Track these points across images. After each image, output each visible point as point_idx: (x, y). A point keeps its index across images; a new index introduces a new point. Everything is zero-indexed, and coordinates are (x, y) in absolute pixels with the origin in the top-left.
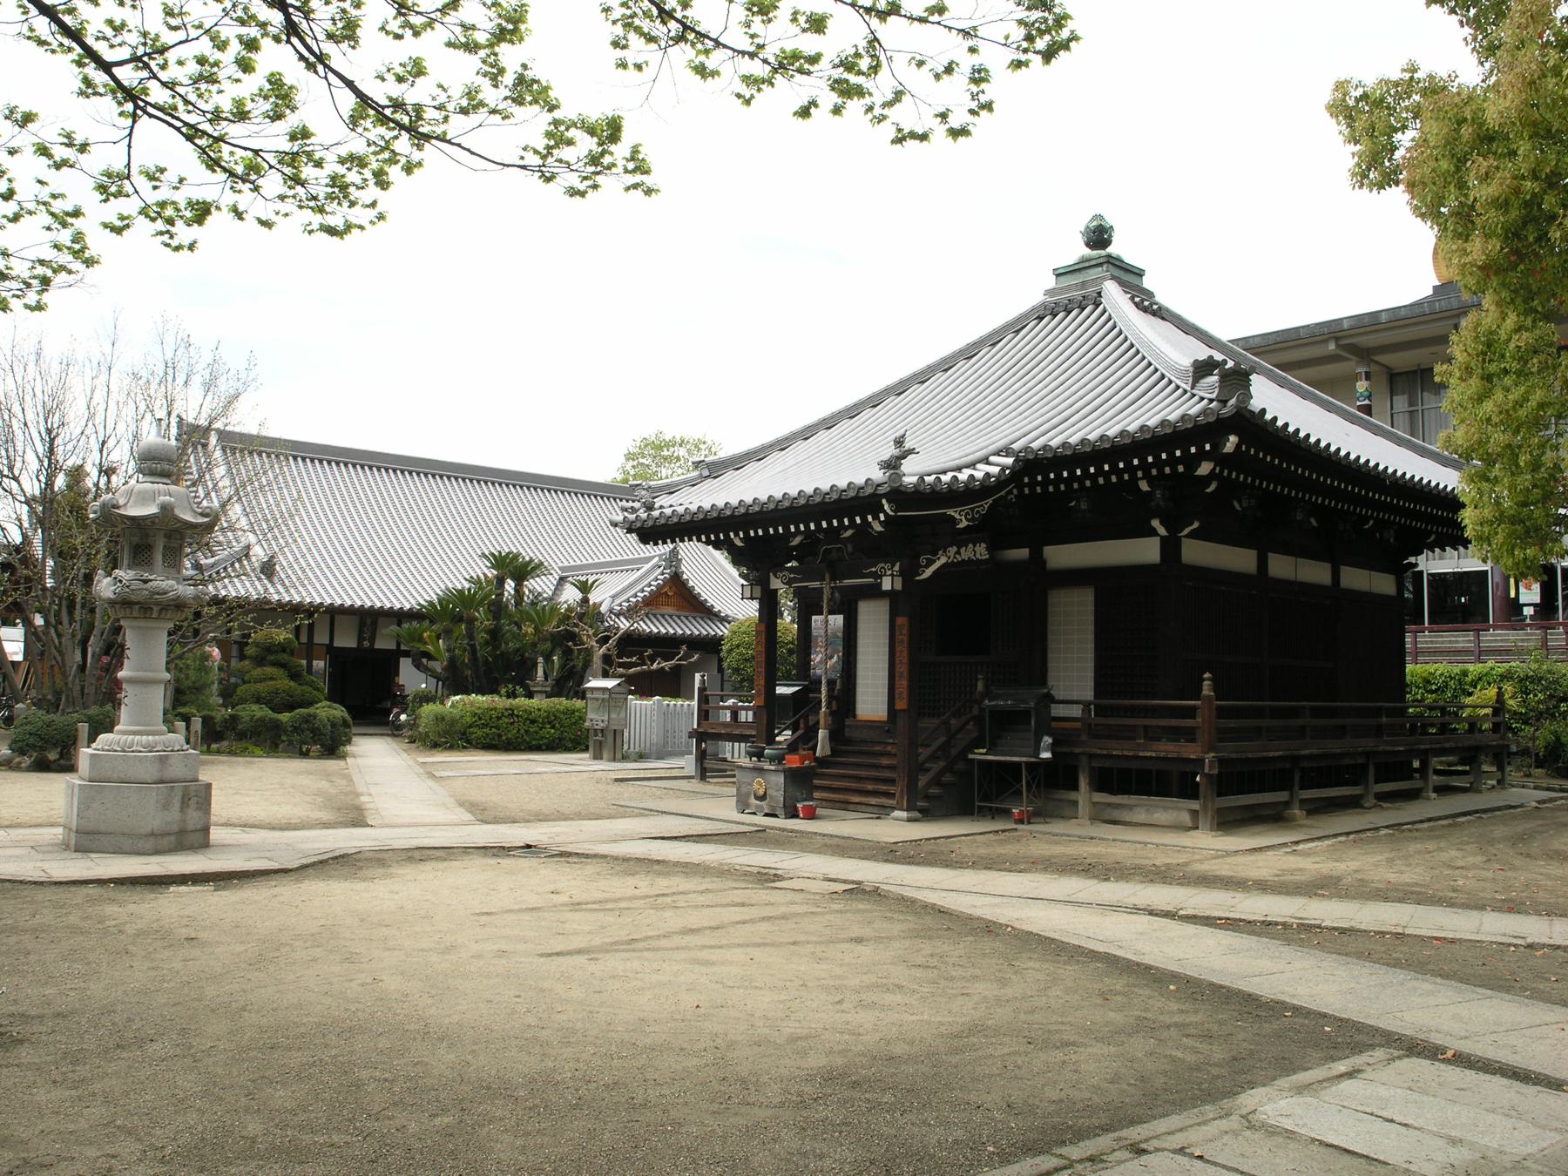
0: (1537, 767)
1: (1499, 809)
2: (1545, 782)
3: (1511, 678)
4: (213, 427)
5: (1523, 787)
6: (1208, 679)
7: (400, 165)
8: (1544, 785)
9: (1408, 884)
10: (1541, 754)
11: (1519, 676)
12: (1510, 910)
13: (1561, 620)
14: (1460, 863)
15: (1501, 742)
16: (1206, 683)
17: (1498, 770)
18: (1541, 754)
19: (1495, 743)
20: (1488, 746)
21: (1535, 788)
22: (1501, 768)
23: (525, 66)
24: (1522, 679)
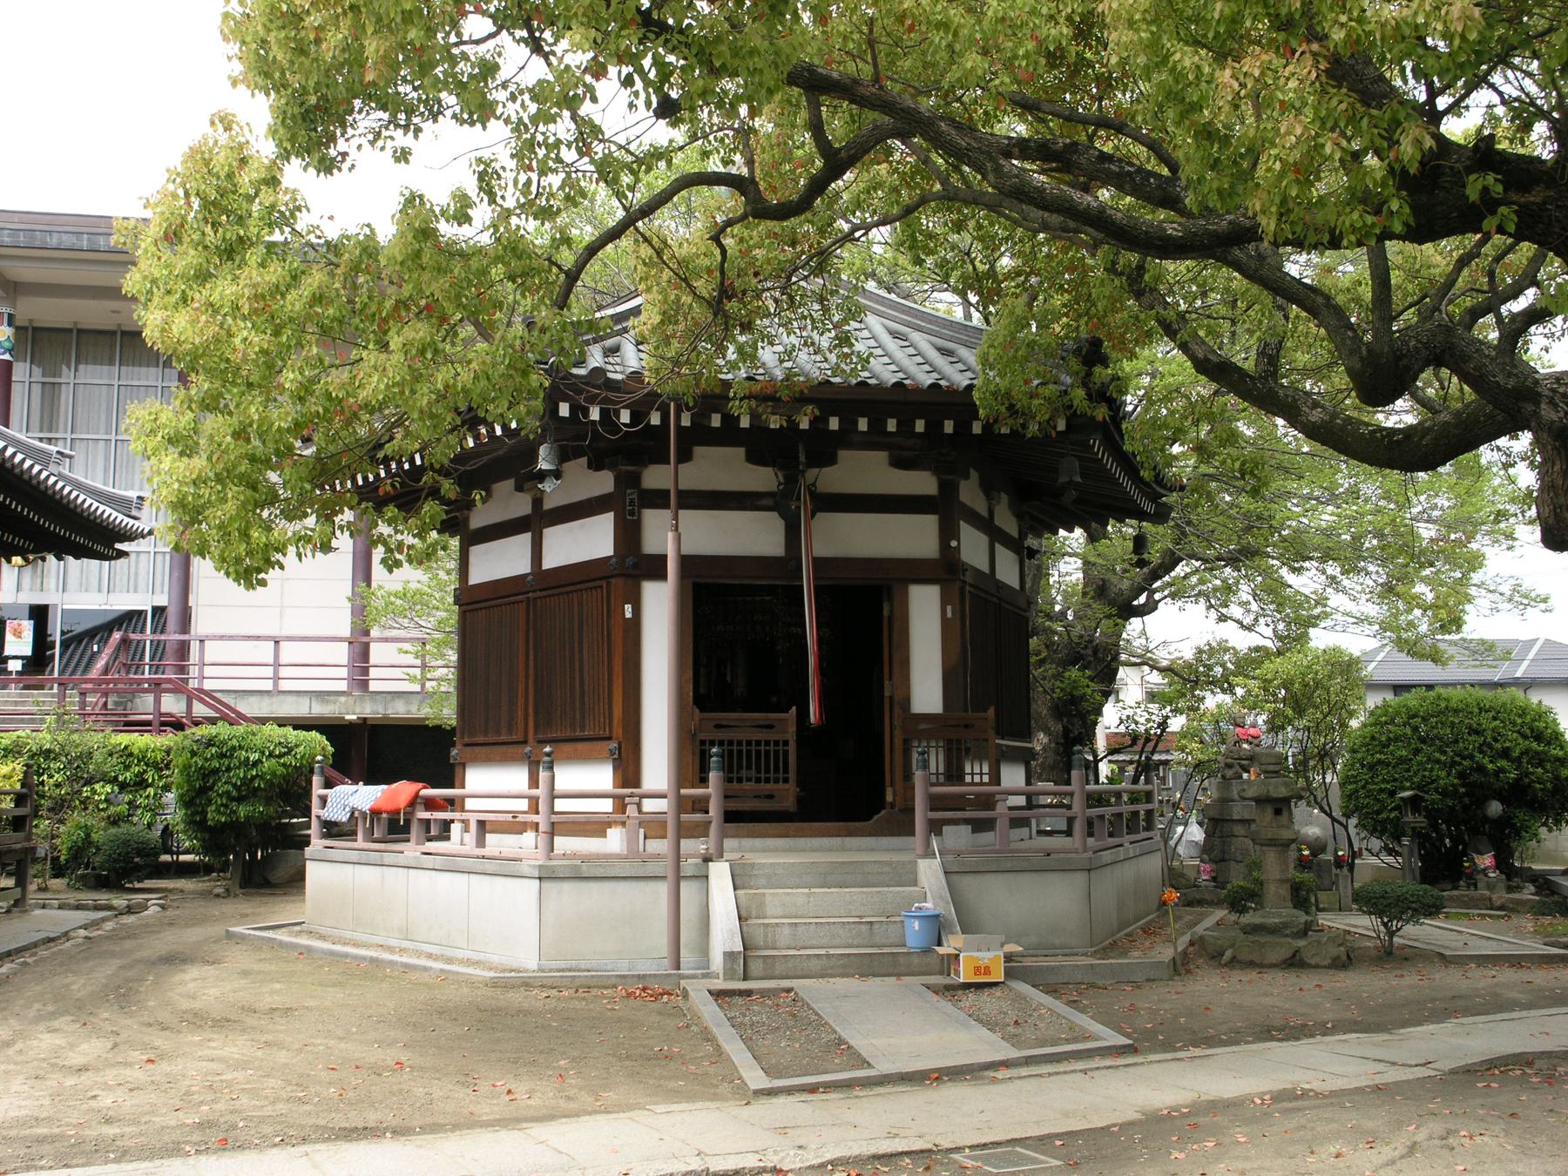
0: (56, 876)
1: (35, 945)
2: (73, 897)
3: (19, 753)
4: (1510, 241)
5: (44, 907)
6: (716, 755)
7: (594, 83)
8: (72, 901)
9: (21, 1123)
10: (62, 858)
11: (30, 750)
12: (224, 1145)
13: (56, 674)
14: (76, 1059)
15: (26, 844)
16: (714, 759)
17: (17, 885)
18: (62, 858)
19: (18, 846)
20: (10, 851)
21: (60, 907)
22: (21, 883)
23: (234, 83)
24: (35, 754)
